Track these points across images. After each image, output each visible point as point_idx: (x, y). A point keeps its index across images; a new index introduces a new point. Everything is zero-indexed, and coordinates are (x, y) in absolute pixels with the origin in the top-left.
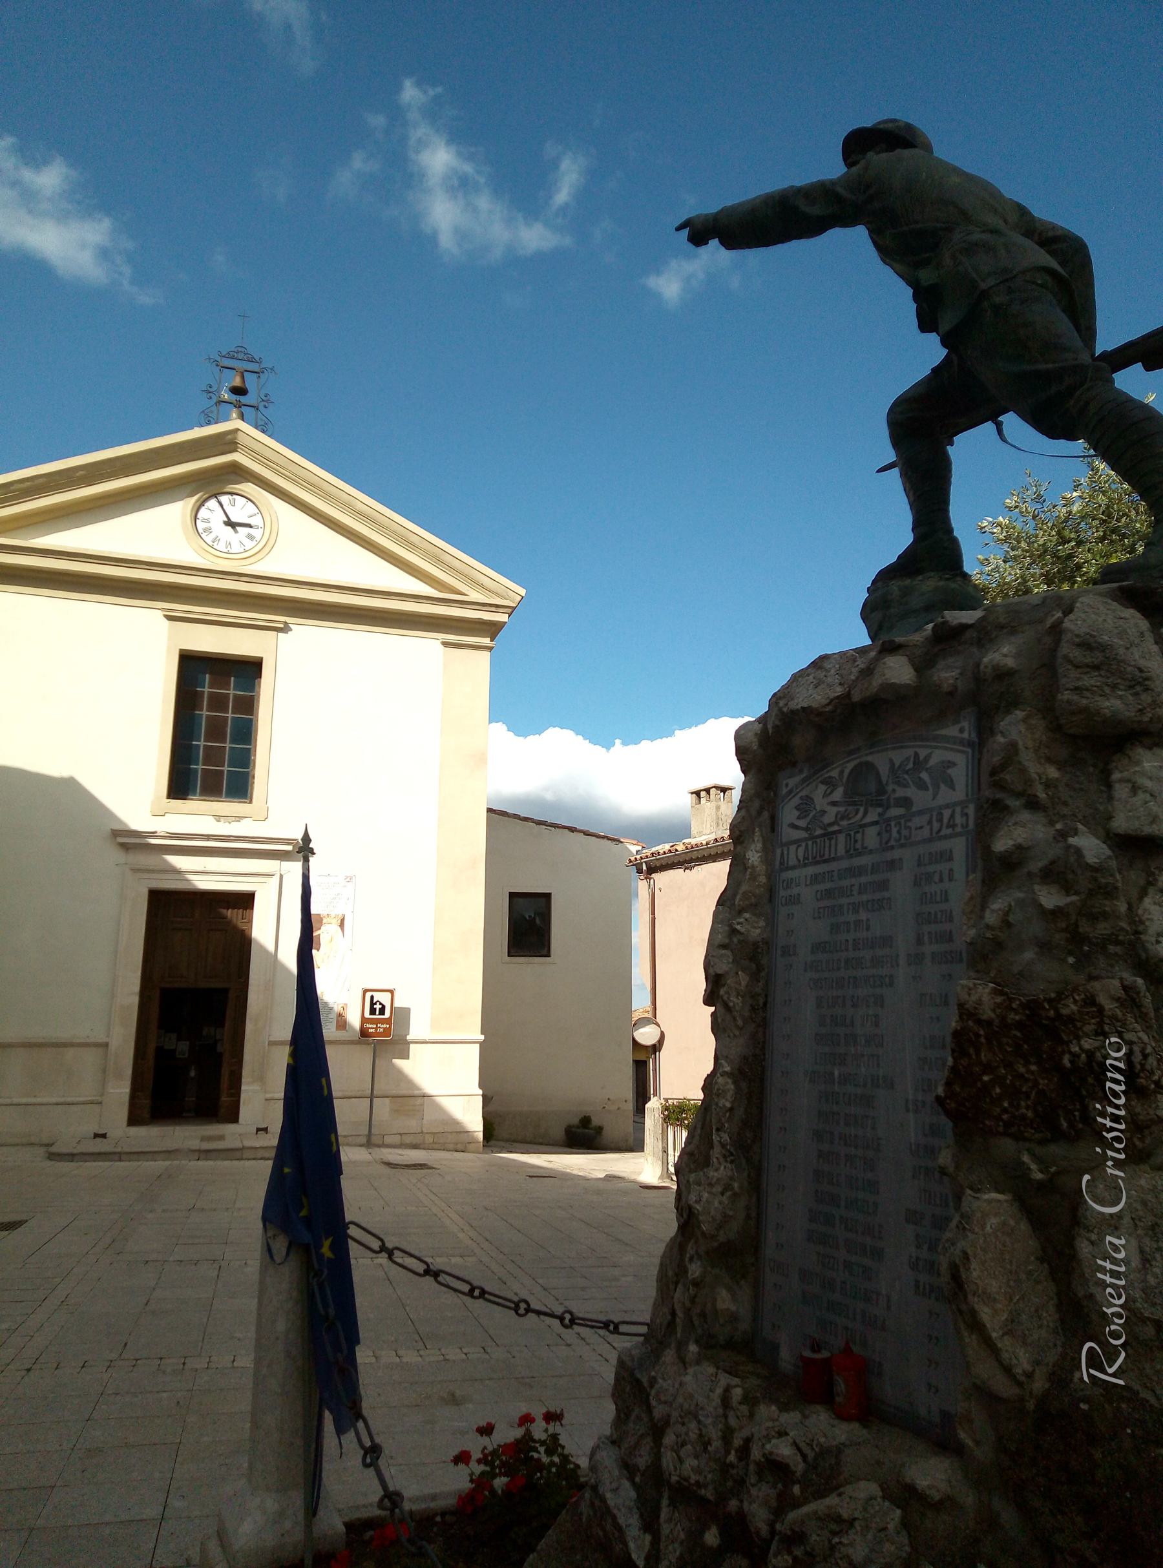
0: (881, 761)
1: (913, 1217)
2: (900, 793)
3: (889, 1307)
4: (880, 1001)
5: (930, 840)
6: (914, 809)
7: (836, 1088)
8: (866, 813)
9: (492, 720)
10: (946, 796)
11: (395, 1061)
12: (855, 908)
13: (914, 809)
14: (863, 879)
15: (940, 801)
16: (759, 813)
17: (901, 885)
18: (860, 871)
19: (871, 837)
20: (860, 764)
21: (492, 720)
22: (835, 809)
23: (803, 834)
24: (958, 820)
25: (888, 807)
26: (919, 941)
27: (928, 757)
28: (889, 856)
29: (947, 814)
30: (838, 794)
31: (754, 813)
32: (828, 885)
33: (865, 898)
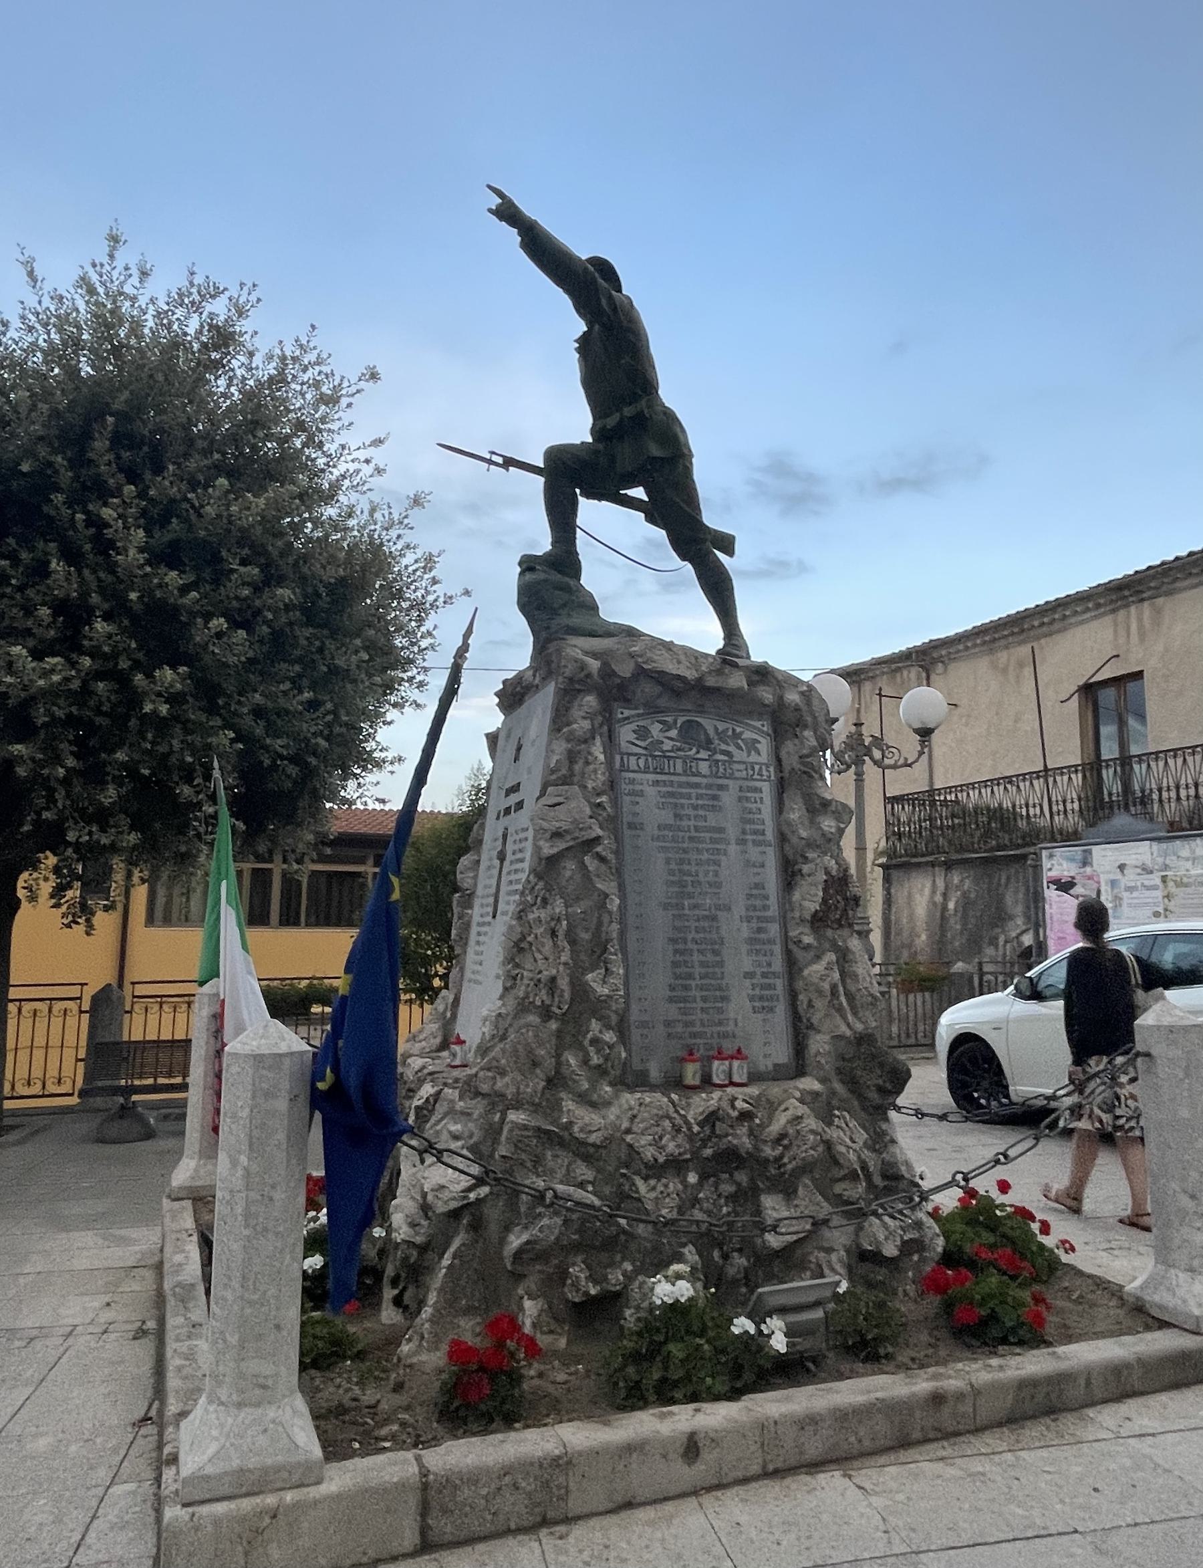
0: (709, 724)
1: (666, 907)
2: (724, 747)
3: (736, 1025)
4: (717, 863)
5: (746, 779)
6: (852, 804)
7: (687, 912)
8: (698, 752)
9: (497, 694)
10: (754, 758)
11: (646, 499)
12: (695, 807)
13: (852, 804)
14: (700, 791)
15: (751, 759)
16: (601, 725)
17: (728, 799)
18: (697, 786)
19: (704, 767)
20: (688, 721)
21: (497, 694)
22: (672, 743)
23: (644, 752)
24: (765, 773)
25: (716, 753)
26: (744, 832)
27: (741, 733)
28: (720, 781)
29: (757, 767)
30: (674, 733)
31: (597, 725)
32: (670, 789)
33: (700, 802)
